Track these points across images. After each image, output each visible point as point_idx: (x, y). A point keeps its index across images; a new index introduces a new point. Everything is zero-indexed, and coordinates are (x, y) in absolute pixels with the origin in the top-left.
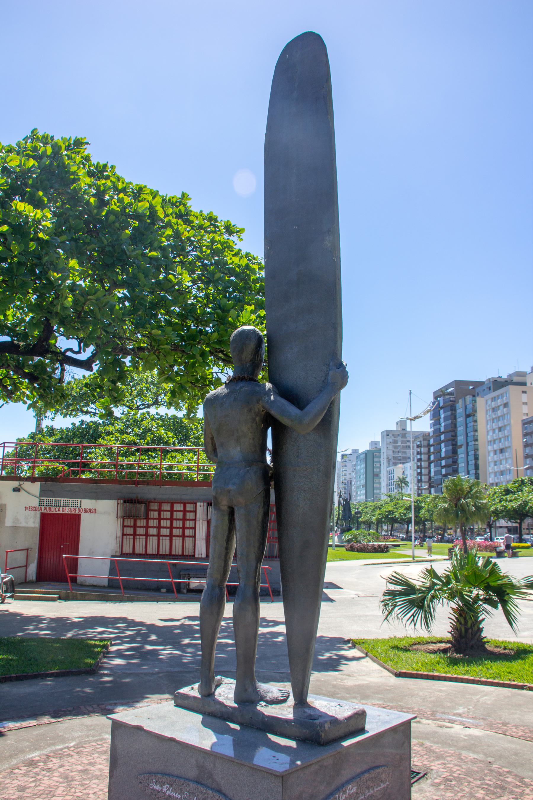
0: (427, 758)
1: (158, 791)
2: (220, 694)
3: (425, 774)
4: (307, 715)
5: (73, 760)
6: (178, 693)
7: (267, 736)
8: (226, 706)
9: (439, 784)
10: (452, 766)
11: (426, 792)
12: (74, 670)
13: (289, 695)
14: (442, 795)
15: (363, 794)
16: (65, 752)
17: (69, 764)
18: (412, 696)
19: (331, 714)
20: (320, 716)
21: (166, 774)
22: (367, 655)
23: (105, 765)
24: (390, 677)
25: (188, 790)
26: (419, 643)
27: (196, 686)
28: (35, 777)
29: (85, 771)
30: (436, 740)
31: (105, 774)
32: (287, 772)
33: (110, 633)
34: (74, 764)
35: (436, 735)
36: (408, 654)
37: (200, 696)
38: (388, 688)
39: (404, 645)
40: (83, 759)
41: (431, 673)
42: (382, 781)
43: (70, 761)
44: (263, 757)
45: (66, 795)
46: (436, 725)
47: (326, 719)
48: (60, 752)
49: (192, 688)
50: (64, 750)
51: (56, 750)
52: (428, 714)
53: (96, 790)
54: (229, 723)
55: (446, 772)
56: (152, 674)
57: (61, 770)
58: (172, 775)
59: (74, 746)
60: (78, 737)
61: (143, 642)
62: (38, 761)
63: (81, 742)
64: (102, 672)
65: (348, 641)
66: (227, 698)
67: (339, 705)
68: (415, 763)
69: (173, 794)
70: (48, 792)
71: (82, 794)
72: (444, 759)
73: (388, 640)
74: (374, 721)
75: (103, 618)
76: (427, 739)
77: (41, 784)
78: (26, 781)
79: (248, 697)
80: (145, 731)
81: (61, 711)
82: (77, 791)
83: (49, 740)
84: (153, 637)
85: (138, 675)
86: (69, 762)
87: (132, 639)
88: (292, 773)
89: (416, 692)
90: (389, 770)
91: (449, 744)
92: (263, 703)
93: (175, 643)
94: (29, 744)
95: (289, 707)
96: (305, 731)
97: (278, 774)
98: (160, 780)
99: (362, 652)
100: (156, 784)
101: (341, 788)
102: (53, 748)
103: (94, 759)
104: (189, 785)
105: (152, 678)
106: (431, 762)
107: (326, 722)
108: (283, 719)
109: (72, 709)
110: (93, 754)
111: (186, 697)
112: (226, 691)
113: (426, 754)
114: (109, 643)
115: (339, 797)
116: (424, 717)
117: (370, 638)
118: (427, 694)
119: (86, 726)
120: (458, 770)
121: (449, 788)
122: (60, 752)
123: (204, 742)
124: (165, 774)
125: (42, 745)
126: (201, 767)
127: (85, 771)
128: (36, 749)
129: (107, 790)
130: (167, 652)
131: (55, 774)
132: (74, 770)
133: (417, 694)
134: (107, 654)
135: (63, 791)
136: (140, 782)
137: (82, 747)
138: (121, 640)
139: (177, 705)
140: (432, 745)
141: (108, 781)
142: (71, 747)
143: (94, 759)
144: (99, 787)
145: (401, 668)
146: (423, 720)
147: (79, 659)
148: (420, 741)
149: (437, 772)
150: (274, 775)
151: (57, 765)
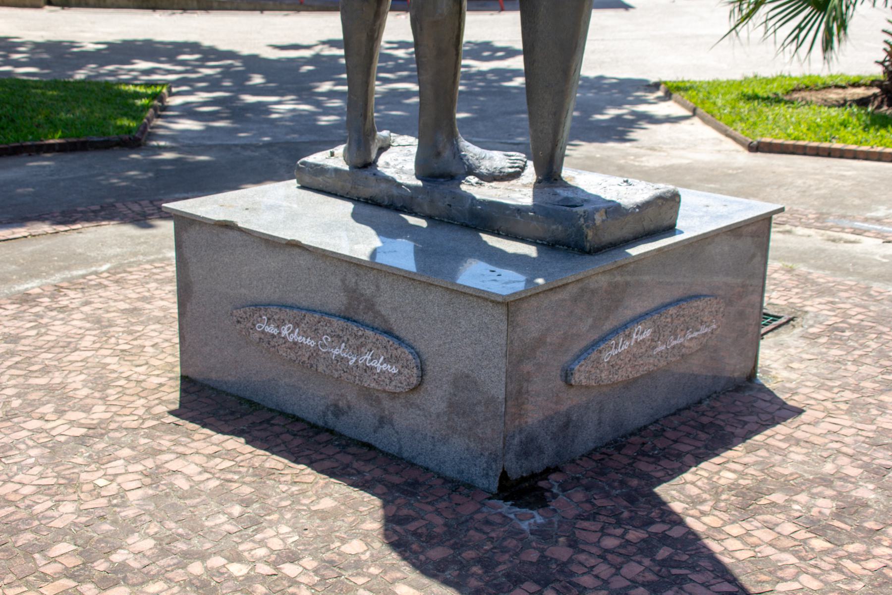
0: (797, 293)
1: (273, 335)
2: (388, 164)
3: (792, 319)
4: (560, 198)
5: (108, 293)
6: (304, 163)
7: (481, 238)
8: (400, 185)
9: (818, 336)
10: (848, 306)
11: (789, 347)
12: (95, 139)
13: (525, 166)
14: (821, 353)
15: (664, 342)
16: (91, 280)
17: (101, 299)
18: (780, 186)
19: (608, 198)
20: (586, 201)
21: (286, 307)
22: (694, 112)
23: (172, 301)
24: (738, 151)
25: (329, 331)
26: (807, 87)
27: (340, 150)
28: (35, 321)
29: (133, 311)
30: (820, 262)
31: (173, 315)
32: (518, 297)
33: (166, 72)
34: (112, 300)
35: (823, 255)
36: (781, 109)
37: (347, 168)
38: (730, 172)
39: (774, 91)
40: (127, 292)
41: (826, 145)
42: (702, 323)
43: (103, 294)
44: (475, 274)
45: (100, 348)
46: (825, 237)
47: (598, 206)
48: (82, 280)
49: (332, 154)
50: (88, 278)
51: (73, 278)
52: (809, 219)
53: (156, 340)
54: (403, 215)
55: (835, 316)
56: (257, 147)
57: (86, 309)
58: (298, 308)
59: (108, 271)
60: (116, 256)
61: (235, 89)
62: (39, 296)
63: (121, 265)
64: (155, 143)
65: (656, 86)
66: (402, 171)
67: (626, 182)
68: (772, 301)
69: (300, 339)
70: (65, 344)
71: (129, 346)
72: (833, 295)
73: (741, 82)
74: (696, 214)
75: (149, 43)
76: (803, 260)
77: (49, 332)
78: (18, 328)
79: (441, 169)
80: (240, 230)
81: (76, 212)
82: (121, 341)
83: (57, 261)
84: (257, 80)
85: (228, 148)
86: (101, 297)
87: (213, 84)
88: (526, 297)
89: (790, 180)
90: (718, 303)
91: (848, 270)
92: (473, 179)
93: (304, 92)
94: (18, 268)
95: (525, 186)
96: (554, 227)
97: (500, 300)
98: (276, 317)
99: (684, 105)
100: (268, 324)
101: (624, 328)
102: (67, 274)
103: (149, 291)
104: (330, 322)
105: (257, 154)
106: (805, 299)
107: (597, 210)
108: (513, 206)
109: (97, 208)
110: (147, 283)
111: (319, 170)
112: (400, 159)
113: (797, 286)
114: (165, 90)
115: (617, 344)
116: (801, 223)
117: (702, 79)
118: (812, 182)
119: (129, 237)
120: (860, 313)
121: (836, 342)
122: (82, 280)
123: (356, 247)
124: (282, 306)
125: (43, 268)
126: (353, 294)
127: (134, 311)
128: (32, 277)
129: (177, 340)
130: (284, 106)
131: (74, 316)
132: (111, 309)
133: (791, 183)
134: (162, 110)
135: (94, 342)
136: (238, 322)
137: (125, 272)
138: (190, 86)
139: (303, 187)
140: (811, 271)
141: (177, 327)
142: (101, 273)
143: (149, 291)
144: (163, 336)
145: (762, 136)
146: (799, 228)
147: (105, 119)
148: (786, 263)
149: (816, 316)
150: (492, 301)
151: (76, 303)
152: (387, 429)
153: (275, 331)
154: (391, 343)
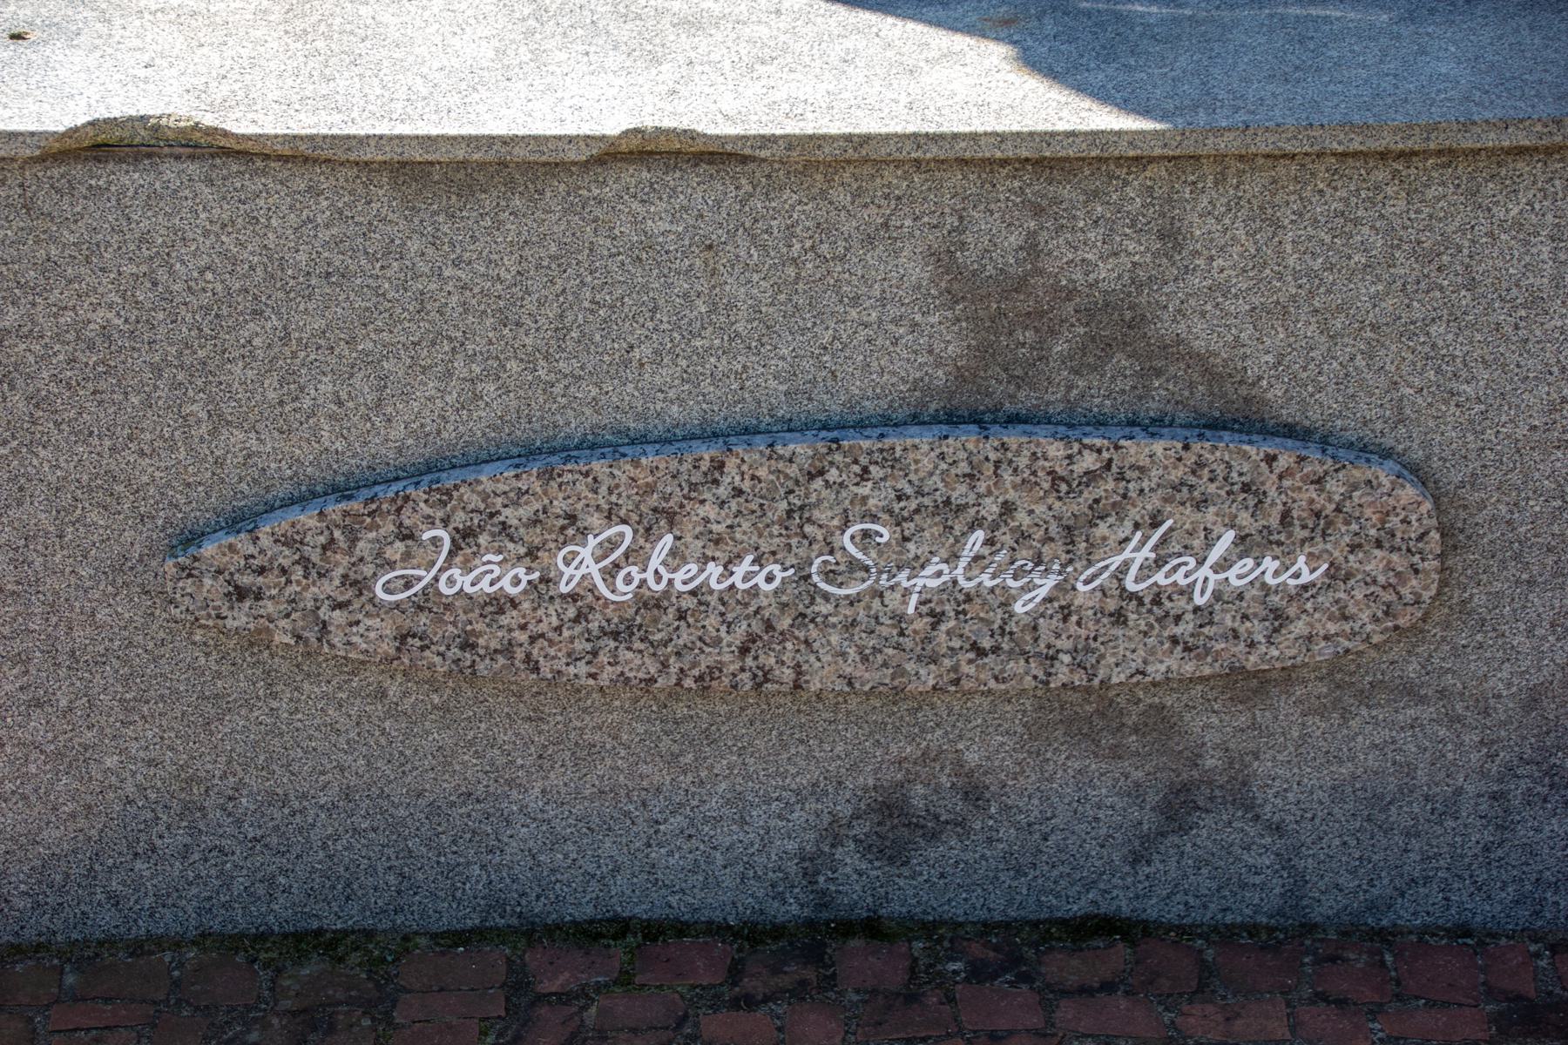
104: (891, 461)
152: (1207, 831)
153: (512, 579)
154: (1284, 461)
